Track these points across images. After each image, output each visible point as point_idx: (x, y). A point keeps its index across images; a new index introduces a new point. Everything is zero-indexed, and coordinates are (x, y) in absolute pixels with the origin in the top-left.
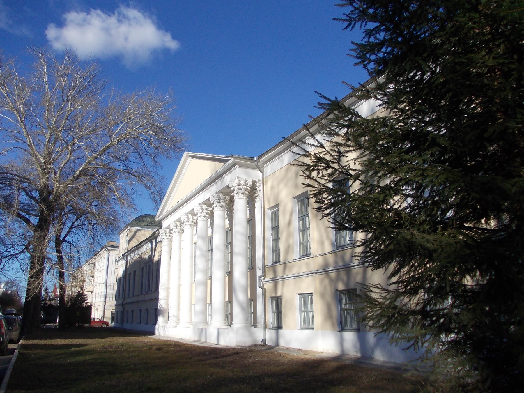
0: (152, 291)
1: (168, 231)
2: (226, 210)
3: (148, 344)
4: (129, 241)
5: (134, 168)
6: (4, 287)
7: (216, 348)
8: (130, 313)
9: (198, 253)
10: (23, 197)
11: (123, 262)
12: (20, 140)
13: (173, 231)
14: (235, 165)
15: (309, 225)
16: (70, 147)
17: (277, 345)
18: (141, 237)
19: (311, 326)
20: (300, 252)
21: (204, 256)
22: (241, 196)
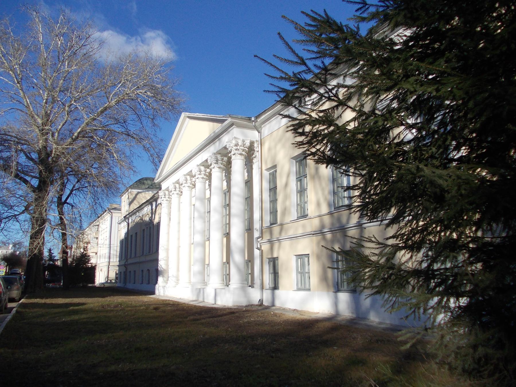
0: (153, 252)
1: (167, 193)
2: (224, 171)
3: (146, 303)
4: (130, 204)
5: (132, 129)
6: (12, 248)
7: (212, 307)
8: (132, 273)
9: (196, 214)
10: (22, 159)
11: (125, 224)
12: (17, 101)
13: (172, 193)
14: (232, 125)
15: (307, 186)
16: (67, 108)
17: (273, 305)
18: (141, 199)
19: (307, 287)
20: (298, 213)
21: (202, 217)
22: (239, 157)
